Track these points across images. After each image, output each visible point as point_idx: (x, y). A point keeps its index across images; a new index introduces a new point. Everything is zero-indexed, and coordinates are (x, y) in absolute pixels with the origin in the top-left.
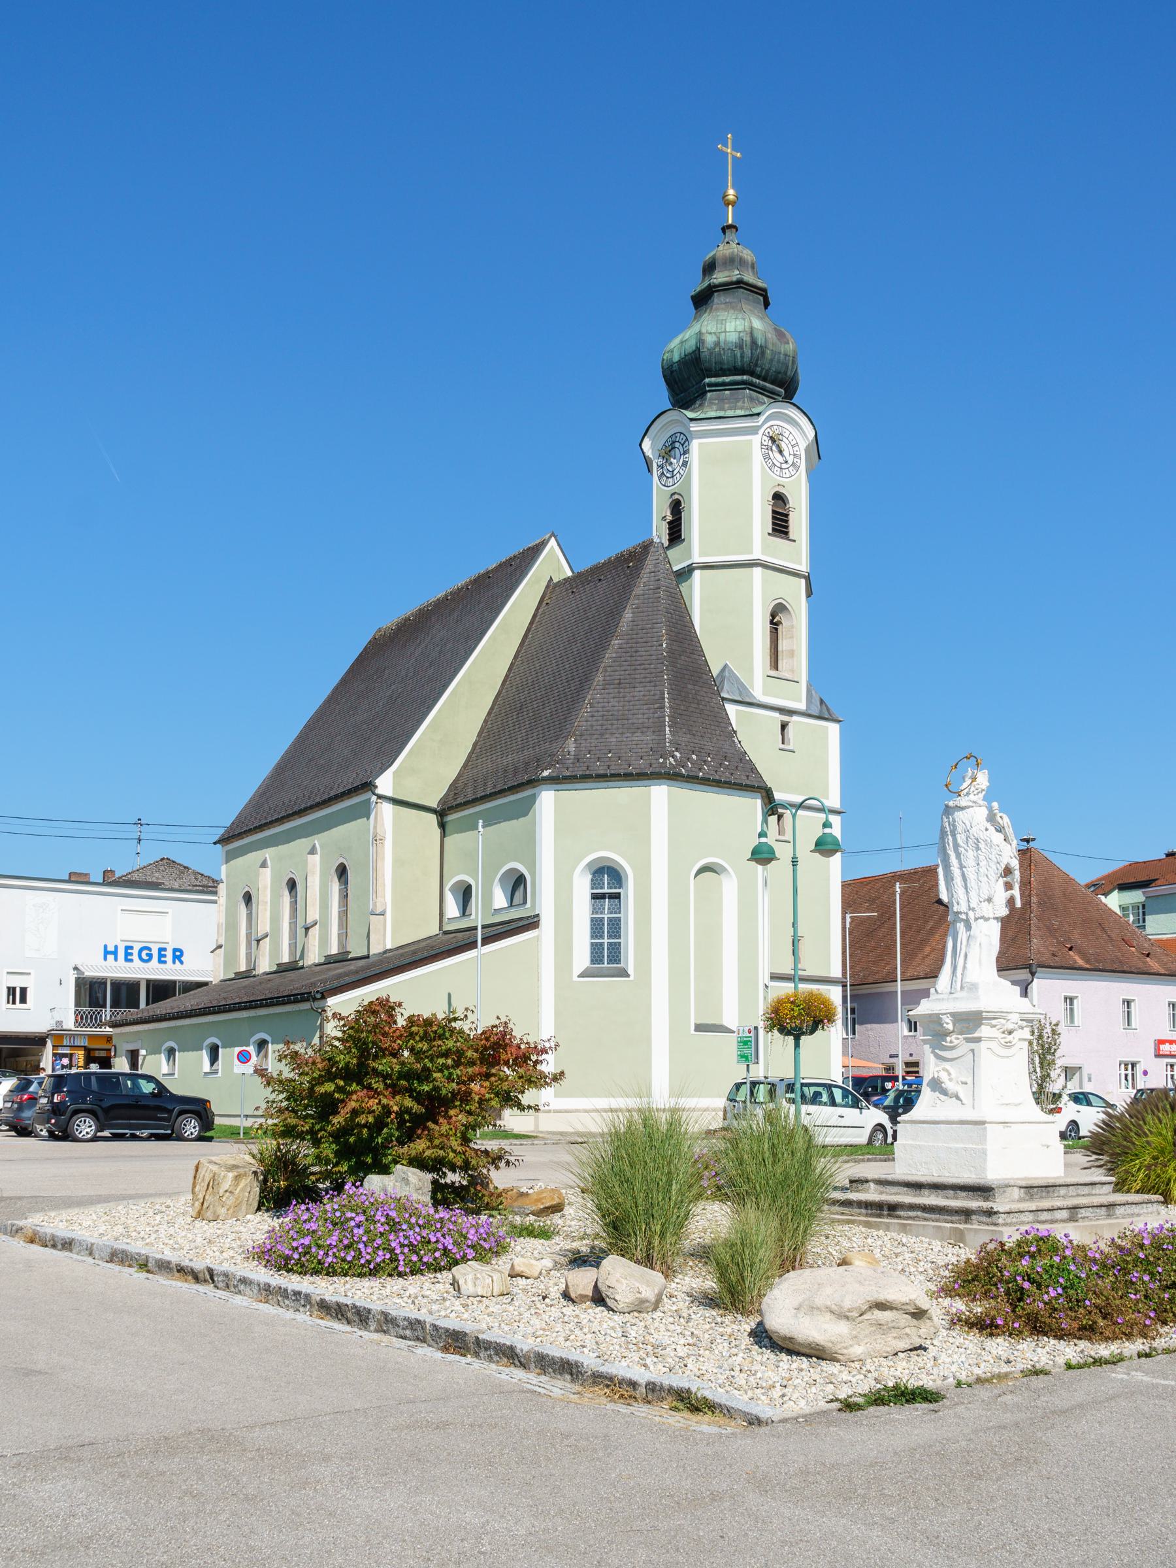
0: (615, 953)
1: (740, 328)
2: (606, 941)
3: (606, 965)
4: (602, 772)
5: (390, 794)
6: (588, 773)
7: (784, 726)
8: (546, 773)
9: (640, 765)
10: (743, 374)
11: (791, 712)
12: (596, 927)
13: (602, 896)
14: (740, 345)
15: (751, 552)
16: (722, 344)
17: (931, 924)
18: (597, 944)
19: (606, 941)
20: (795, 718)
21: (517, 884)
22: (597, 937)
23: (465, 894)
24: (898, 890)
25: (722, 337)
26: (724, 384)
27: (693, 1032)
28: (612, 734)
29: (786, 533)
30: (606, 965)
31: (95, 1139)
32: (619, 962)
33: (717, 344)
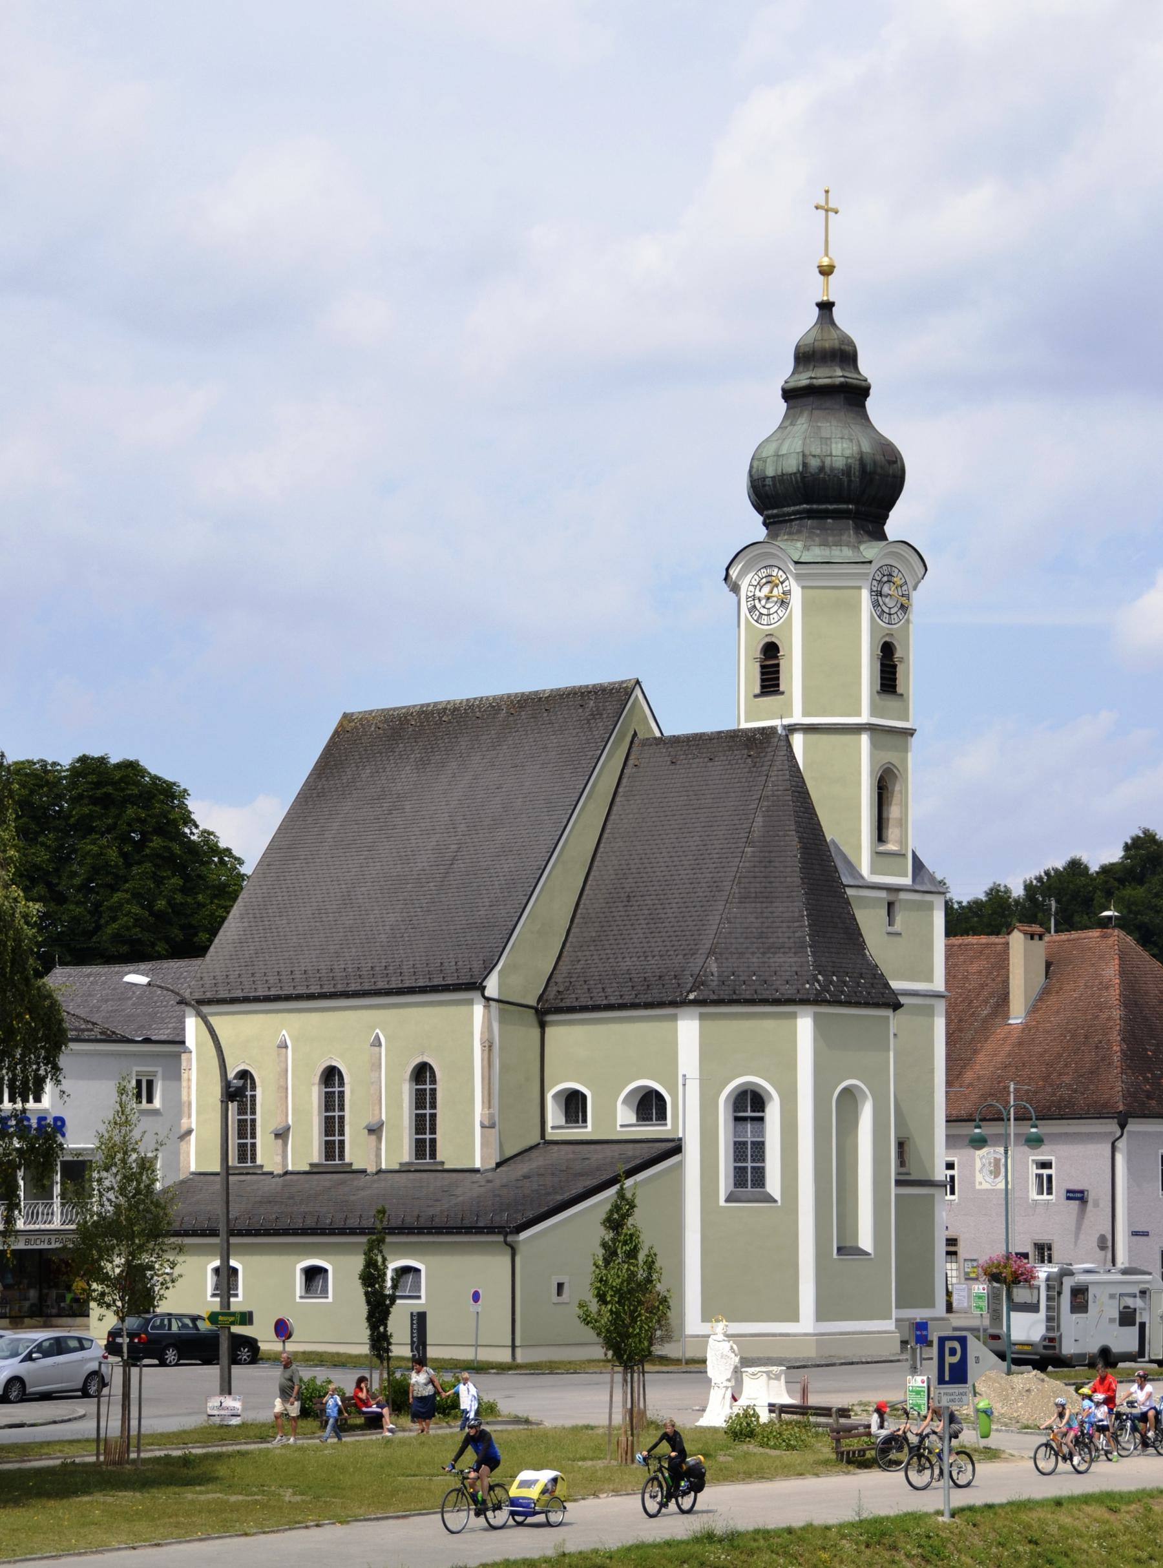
0: (759, 1178)
1: (848, 453)
2: (749, 1165)
3: (749, 1189)
4: (748, 997)
5: (496, 996)
6: (735, 997)
7: (890, 905)
8: (691, 996)
9: (788, 991)
10: (848, 503)
11: (896, 890)
12: (739, 1150)
13: (745, 1119)
14: (848, 470)
15: (859, 715)
16: (827, 470)
17: (969, 1035)
18: (740, 1168)
19: (749, 1165)
20: (903, 896)
21: (650, 1105)
22: (759, 1168)
23: (574, 1104)
24: (1012, 1089)
25: (828, 461)
26: (827, 511)
27: (835, 1255)
28: (753, 953)
29: (895, 686)
30: (749, 1189)
31: (177, 1365)
32: (326, 1093)
33: (822, 469)
